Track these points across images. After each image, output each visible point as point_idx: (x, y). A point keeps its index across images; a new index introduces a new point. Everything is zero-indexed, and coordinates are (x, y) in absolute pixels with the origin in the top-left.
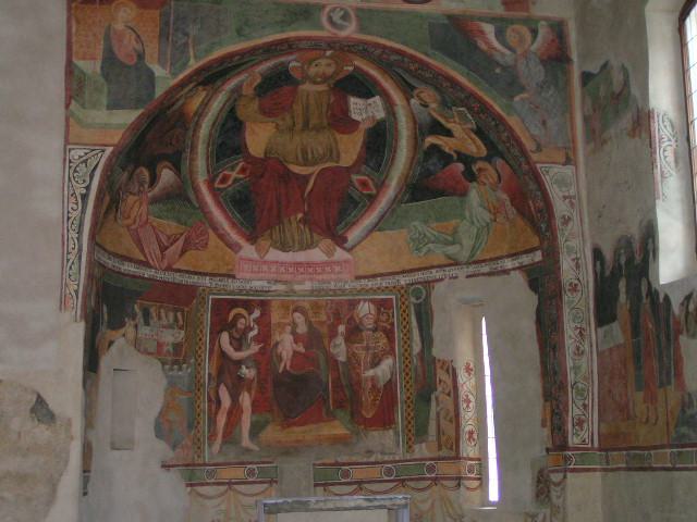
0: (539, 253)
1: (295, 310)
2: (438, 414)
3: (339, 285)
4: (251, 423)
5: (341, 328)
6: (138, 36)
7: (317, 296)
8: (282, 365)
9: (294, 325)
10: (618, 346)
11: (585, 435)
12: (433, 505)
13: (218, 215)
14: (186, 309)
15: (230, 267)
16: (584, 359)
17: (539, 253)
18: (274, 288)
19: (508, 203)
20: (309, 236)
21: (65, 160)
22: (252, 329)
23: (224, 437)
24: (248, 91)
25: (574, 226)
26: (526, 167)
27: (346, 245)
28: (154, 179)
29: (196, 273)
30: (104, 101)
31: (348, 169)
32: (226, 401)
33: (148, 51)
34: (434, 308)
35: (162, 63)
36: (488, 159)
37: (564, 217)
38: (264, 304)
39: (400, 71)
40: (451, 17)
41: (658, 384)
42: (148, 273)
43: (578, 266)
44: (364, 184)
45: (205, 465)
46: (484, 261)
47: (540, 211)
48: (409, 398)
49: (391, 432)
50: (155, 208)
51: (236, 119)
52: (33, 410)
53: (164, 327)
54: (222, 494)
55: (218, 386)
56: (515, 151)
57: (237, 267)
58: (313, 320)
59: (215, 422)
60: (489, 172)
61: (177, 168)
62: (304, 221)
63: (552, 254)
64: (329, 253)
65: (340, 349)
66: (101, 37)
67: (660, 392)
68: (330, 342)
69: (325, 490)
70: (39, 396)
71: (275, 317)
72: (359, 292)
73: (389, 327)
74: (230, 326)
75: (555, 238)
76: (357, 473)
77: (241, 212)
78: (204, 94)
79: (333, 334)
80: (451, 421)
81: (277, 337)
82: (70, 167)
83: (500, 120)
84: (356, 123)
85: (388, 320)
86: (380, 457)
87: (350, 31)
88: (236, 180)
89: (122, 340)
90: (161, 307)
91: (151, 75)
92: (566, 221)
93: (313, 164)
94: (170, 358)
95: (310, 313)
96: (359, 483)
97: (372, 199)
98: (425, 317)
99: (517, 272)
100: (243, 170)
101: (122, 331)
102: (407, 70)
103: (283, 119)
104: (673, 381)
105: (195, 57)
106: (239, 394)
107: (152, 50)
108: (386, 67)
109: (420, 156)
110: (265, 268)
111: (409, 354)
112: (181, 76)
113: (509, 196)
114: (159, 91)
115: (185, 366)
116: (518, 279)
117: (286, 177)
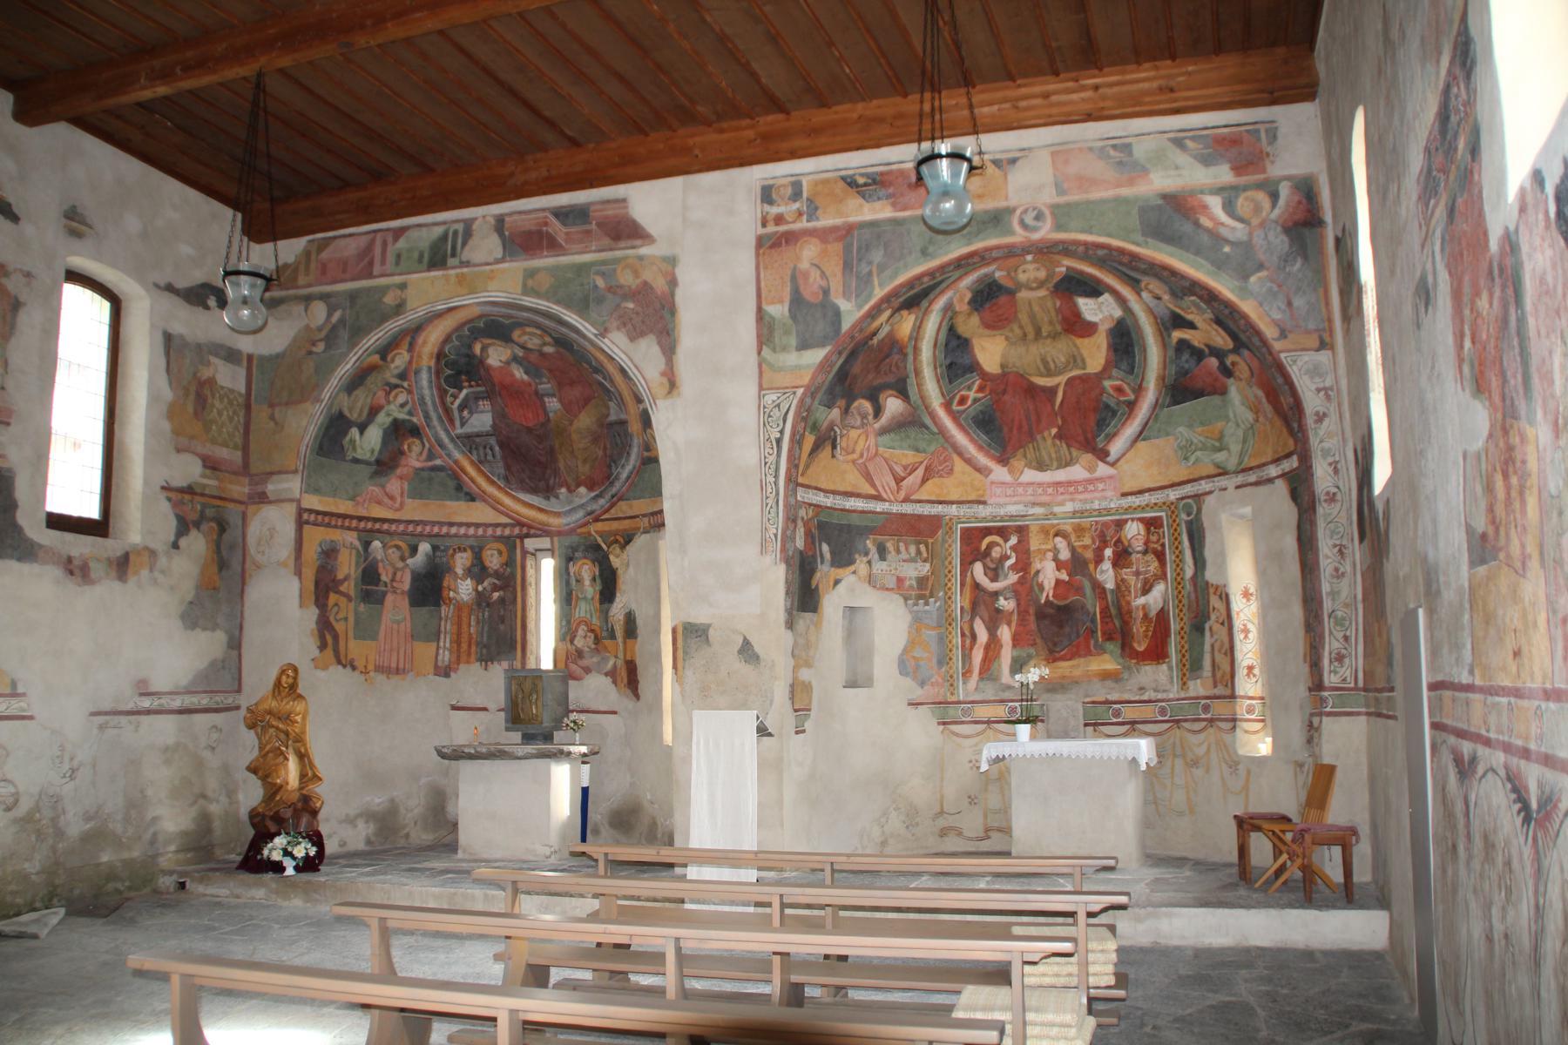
0: (1295, 458)
1: (1056, 535)
2: (1212, 646)
3: (1104, 504)
4: (1013, 658)
5: (1108, 552)
8: (1044, 595)
9: (1056, 551)
11: (1346, 672)
12: (1209, 749)
13: (960, 438)
14: (930, 541)
15: (981, 492)
16: (1345, 583)
17: (1295, 458)
19: (1264, 400)
20: (1067, 453)
22: (1008, 558)
23: (980, 674)
24: (962, 307)
27: (1109, 459)
28: (878, 411)
29: (940, 502)
30: (793, 341)
32: (983, 636)
33: (832, 289)
34: (1205, 525)
36: (1236, 350)
37: (1317, 414)
38: (1022, 531)
39: (1115, 265)
40: (1165, 197)
42: (879, 507)
43: (1336, 471)
44: (1119, 390)
45: (959, 702)
46: (1251, 469)
48: (1182, 629)
49: (1164, 667)
50: (886, 438)
51: (959, 337)
52: (740, 652)
53: (904, 561)
54: (978, 734)
55: (972, 621)
56: (1256, 340)
57: (988, 492)
58: (1076, 544)
60: (1243, 370)
61: (903, 393)
62: (1059, 436)
64: (1091, 469)
65: (1107, 575)
66: (787, 279)
68: (1096, 568)
69: (1095, 730)
70: (745, 639)
71: (1035, 543)
72: (1127, 510)
73: (1159, 548)
76: (1129, 713)
77: (987, 433)
79: (1099, 559)
80: (1225, 654)
81: (1037, 565)
82: (764, 413)
85: (1158, 540)
87: (1045, 232)
88: (976, 400)
89: (853, 578)
90: (898, 541)
91: (837, 313)
92: (1320, 418)
93: (1059, 373)
96: (1133, 723)
97: (1132, 405)
100: (981, 389)
101: (852, 568)
102: (1121, 263)
103: (1012, 331)
106: (998, 628)
107: (836, 285)
108: (1101, 263)
109: (1171, 353)
110: (1020, 490)
112: (867, 308)
113: (1264, 392)
114: (846, 325)
115: (932, 600)
116: (1281, 487)
117: (1032, 391)
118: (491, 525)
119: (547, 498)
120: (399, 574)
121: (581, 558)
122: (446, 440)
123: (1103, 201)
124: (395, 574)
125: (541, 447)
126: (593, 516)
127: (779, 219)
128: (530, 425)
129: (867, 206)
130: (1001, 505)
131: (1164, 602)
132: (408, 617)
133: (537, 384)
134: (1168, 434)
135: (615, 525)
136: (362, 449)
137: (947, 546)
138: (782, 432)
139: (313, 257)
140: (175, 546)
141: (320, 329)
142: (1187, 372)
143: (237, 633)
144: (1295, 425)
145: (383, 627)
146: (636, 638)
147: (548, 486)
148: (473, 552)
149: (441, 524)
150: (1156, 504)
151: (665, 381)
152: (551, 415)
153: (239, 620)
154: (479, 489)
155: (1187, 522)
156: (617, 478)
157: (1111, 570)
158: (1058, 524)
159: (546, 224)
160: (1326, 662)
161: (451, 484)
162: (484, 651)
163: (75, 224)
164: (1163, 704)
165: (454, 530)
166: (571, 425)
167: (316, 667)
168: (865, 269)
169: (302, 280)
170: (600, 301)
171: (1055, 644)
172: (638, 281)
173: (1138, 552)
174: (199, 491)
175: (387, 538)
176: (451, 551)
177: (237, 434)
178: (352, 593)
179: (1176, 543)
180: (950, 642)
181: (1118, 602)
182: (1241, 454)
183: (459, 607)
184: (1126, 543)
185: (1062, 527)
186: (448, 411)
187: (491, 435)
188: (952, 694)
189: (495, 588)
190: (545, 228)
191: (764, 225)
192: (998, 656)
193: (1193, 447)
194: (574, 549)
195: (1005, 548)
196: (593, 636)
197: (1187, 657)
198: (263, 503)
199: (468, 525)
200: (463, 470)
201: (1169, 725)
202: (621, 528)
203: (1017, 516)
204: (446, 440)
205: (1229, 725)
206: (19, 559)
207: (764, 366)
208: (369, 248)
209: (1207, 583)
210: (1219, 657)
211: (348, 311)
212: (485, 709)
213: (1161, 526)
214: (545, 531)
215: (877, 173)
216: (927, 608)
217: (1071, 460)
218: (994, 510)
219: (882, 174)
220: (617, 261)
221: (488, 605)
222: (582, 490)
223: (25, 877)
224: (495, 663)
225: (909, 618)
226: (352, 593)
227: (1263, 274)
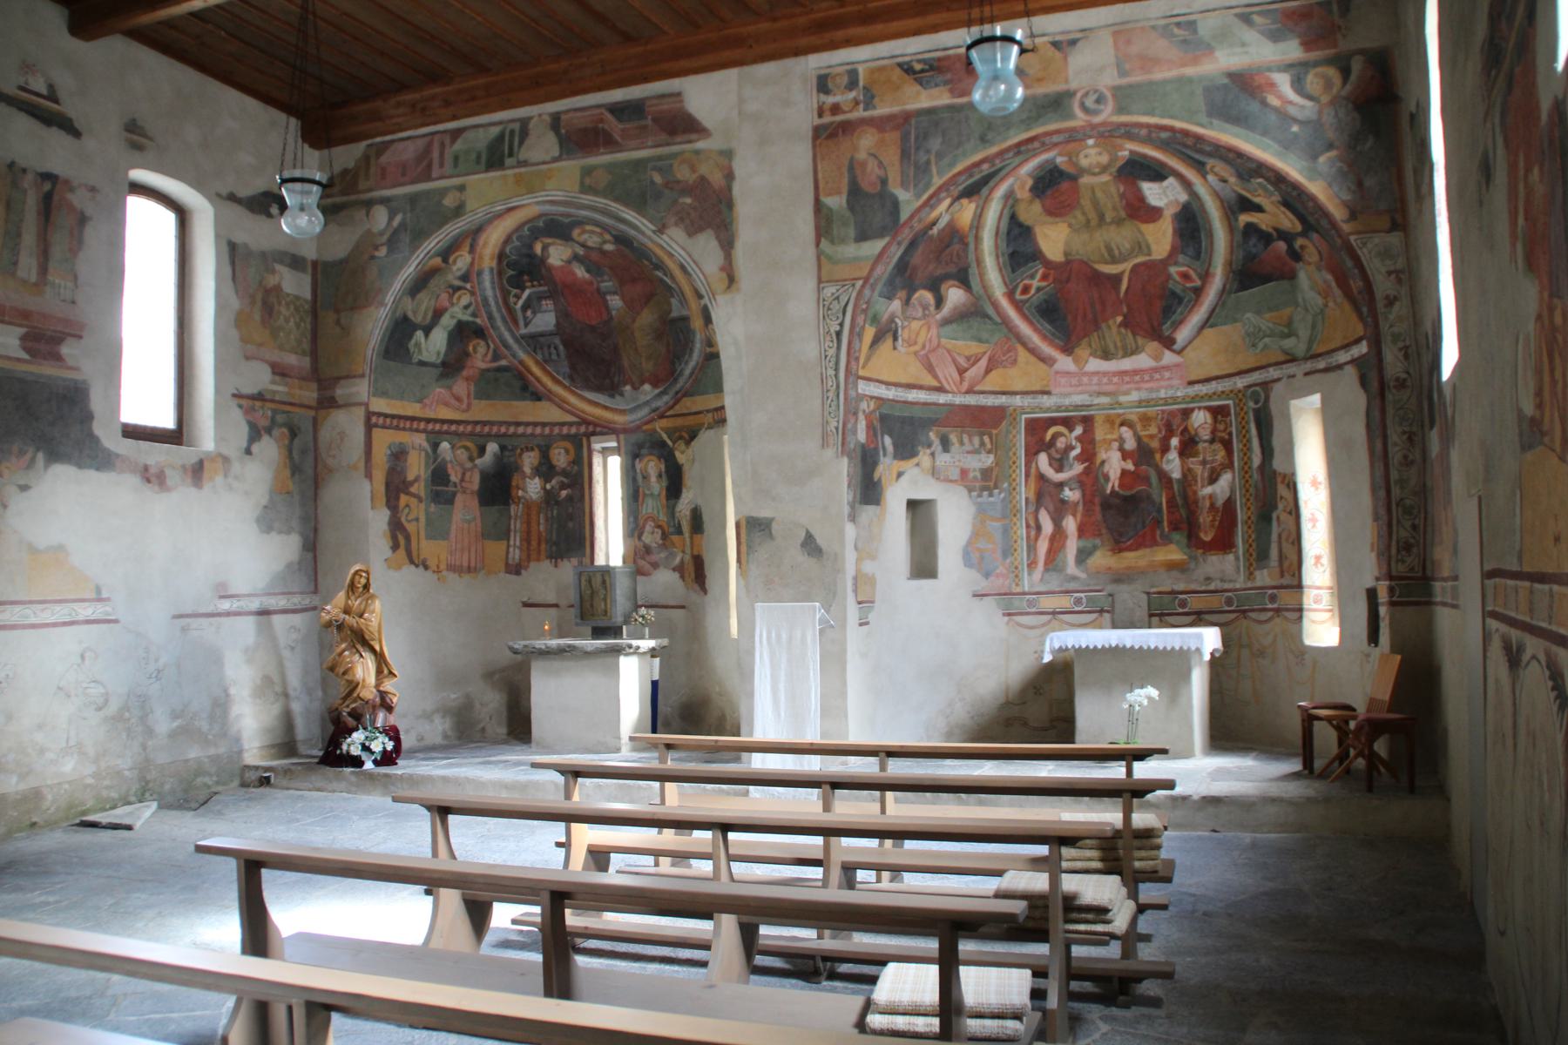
1: (1122, 424)
2: (1280, 536)
3: (1170, 393)
5: (1175, 442)
6: (881, 162)
7: (1145, 407)
8: (1110, 485)
9: (1121, 440)
13: (1024, 328)
14: (994, 432)
15: (1045, 382)
17: (1364, 343)
18: (1096, 401)
19: (1334, 284)
21: (819, 299)
22: (1073, 448)
23: (1046, 564)
24: (1023, 194)
28: (940, 302)
29: (1004, 393)
30: (852, 232)
31: (1165, 263)
35: (904, 185)
36: (1304, 234)
37: (1387, 297)
38: (1087, 421)
42: (942, 399)
44: (1185, 276)
45: (1024, 593)
48: (1249, 518)
49: (1231, 557)
50: (948, 329)
51: (1020, 225)
54: (1043, 625)
56: (1324, 222)
59: (1035, 549)
62: (1125, 324)
64: (1157, 358)
65: (1173, 464)
66: (845, 170)
68: (1162, 458)
69: (1161, 621)
70: (808, 532)
71: (1100, 433)
72: (1194, 399)
73: (1227, 437)
74: (1048, 446)
78: (973, 206)
79: (1165, 449)
80: (1293, 543)
81: (1102, 455)
82: (824, 306)
87: (1107, 114)
88: (1039, 289)
90: (962, 432)
91: (896, 205)
92: (1391, 302)
94: (977, 485)
95: (1139, 427)
97: (1198, 292)
100: (1044, 278)
101: (915, 460)
103: (1075, 217)
105: (938, 173)
107: (894, 175)
109: (1238, 237)
110: (1085, 379)
111: (1250, 468)
115: (996, 491)
116: (1351, 373)
117: (1097, 279)
119: (612, 396)
120: (468, 474)
122: (511, 341)
123: (1165, 82)
126: (657, 413)
127: (836, 109)
129: (924, 94)
130: (1068, 395)
133: (599, 282)
134: (1235, 321)
135: (679, 422)
136: (427, 350)
137: (1011, 436)
138: (841, 325)
140: (248, 452)
141: (381, 234)
143: (312, 535)
148: (540, 451)
149: (508, 424)
150: (1223, 392)
151: (724, 275)
152: (614, 313)
153: (313, 524)
155: (1254, 410)
156: (681, 374)
157: (1177, 462)
158: (1124, 414)
159: (602, 121)
162: (554, 548)
163: (135, 137)
164: (1230, 594)
165: (521, 430)
167: (389, 567)
168: (923, 157)
169: (362, 185)
170: (658, 196)
171: (1121, 535)
172: (694, 176)
173: (1205, 441)
174: (268, 397)
176: (519, 451)
177: (304, 340)
178: (422, 494)
179: (1244, 431)
180: (1015, 533)
182: (1311, 342)
183: (529, 505)
184: (1193, 432)
186: (510, 311)
188: (1017, 585)
189: (563, 486)
190: (600, 125)
192: (1063, 546)
193: (1261, 334)
197: (1254, 545)
199: (535, 424)
202: (687, 423)
203: (1082, 406)
204: (511, 341)
206: (98, 469)
207: (822, 257)
208: (427, 150)
209: (1275, 472)
213: (1229, 414)
214: (610, 429)
215: (933, 59)
216: (991, 499)
217: (1137, 348)
218: (1059, 400)
219: (939, 59)
221: (557, 503)
222: (647, 387)
223: (119, 773)
225: (973, 509)
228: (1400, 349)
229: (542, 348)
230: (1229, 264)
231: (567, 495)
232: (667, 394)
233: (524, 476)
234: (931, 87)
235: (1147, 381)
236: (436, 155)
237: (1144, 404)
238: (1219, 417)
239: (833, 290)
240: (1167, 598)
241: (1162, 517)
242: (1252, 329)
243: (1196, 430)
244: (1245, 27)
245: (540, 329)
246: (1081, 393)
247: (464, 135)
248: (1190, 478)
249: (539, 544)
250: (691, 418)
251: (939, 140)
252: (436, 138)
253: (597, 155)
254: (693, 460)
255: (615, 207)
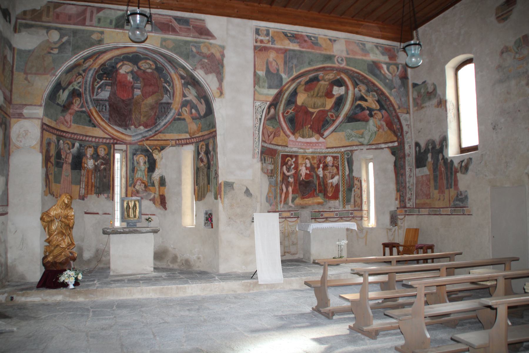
1: (306, 159)
2: (355, 195)
3: (321, 150)
5: (321, 165)
8: (302, 177)
9: (306, 164)
10: (426, 175)
11: (411, 203)
14: (274, 158)
16: (412, 178)
19: (385, 125)
22: (292, 165)
23: (284, 202)
24: (303, 83)
25: (409, 135)
26: (395, 114)
30: (266, 85)
31: (328, 111)
32: (285, 190)
33: (280, 70)
34: (354, 159)
36: (379, 110)
37: (406, 132)
38: (296, 157)
41: (445, 188)
43: (410, 148)
46: (373, 144)
47: (398, 129)
48: (344, 190)
49: (338, 201)
52: (245, 193)
53: (269, 164)
54: (283, 222)
55: (282, 184)
56: (391, 109)
58: (312, 162)
61: (275, 109)
62: (310, 128)
63: (402, 144)
64: (318, 139)
65: (320, 172)
66: (265, 63)
67: (447, 191)
69: (315, 220)
70: (247, 188)
71: (300, 161)
72: (328, 153)
73: (337, 165)
75: (403, 139)
76: (326, 215)
79: (318, 167)
80: (359, 198)
81: (300, 168)
82: (256, 108)
83: (387, 98)
84: (333, 95)
85: (337, 163)
86: (334, 210)
87: (343, 65)
88: (291, 113)
91: (281, 79)
92: (407, 133)
93: (317, 108)
96: (327, 218)
97: (334, 121)
98: (350, 163)
99: (387, 149)
100: (293, 110)
104: (453, 187)
105: (296, 71)
107: (281, 68)
109: (354, 107)
110: (297, 143)
113: (386, 123)
115: (273, 177)
118: (101, 138)
119: (126, 129)
120: (68, 155)
121: (139, 154)
122: (89, 100)
123: (359, 59)
124: (66, 155)
125: (126, 108)
126: (146, 138)
127: (262, 41)
128: (124, 99)
129: (291, 44)
131: (338, 182)
132: (70, 175)
133: (134, 83)
134: (343, 131)
135: (156, 143)
138: (261, 116)
139: (51, 9)
141: (55, 43)
142: (356, 114)
144: (399, 134)
145: (62, 178)
146: (165, 186)
147: (126, 124)
148: (94, 148)
149: (83, 135)
150: (337, 152)
151: (218, 91)
152: (135, 96)
154: (98, 122)
155: (347, 158)
156: (159, 124)
157: (322, 171)
158: (307, 155)
159: (171, 22)
160: (407, 200)
161: (88, 119)
162: (98, 190)
164: (337, 212)
165: (87, 139)
166: (143, 101)
168: (291, 65)
169: (44, 18)
170: (194, 56)
171: (304, 193)
172: (209, 52)
173: (330, 166)
175: (65, 139)
176: (86, 147)
178: (53, 162)
179: (343, 164)
181: (324, 181)
182: (369, 140)
183: (88, 171)
184: (327, 163)
185: (308, 156)
186: (93, 88)
187: (107, 101)
189: (102, 164)
190: (170, 23)
191: (256, 42)
192: (288, 196)
193: (352, 136)
194: (136, 150)
195: (292, 161)
196: (144, 185)
197: (345, 198)
198: (20, 118)
199: (93, 137)
200: (92, 113)
201: (339, 218)
202: (159, 144)
204: (89, 100)
205: (360, 218)
207: (256, 92)
208: (84, 12)
209: (354, 177)
210: (357, 199)
211: (72, 38)
212: (98, 214)
213: (338, 159)
214: (124, 142)
215: (294, 34)
217: (312, 136)
219: (296, 34)
220: (200, 43)
221: (99, 171)
222: (142, 127)
224: (102, 195)
225: (268, 183)
226: (53, 162)
227: (395, 90)
228: (409, 146)
229: (99, 106)
230: (347, 114)
231: (104, 168)
232: (151, 131)
233: (87, 158)
234: (293, 43)
235: (315, 146)
236: (88, 15)
237: (313, 153)
238: (335, 159)
239: (259, 103)
240: (317, 213)
241: (316, 188)
242: (348, 134)
243: (328, 162)
244: (376, 49)
245: (101, 98)
246: (296, 148)
247: (104, 11)
248: (325, 177)
249: (92, 187)
250: (162, 142)
251: (296, 61)
252: (89, 8)
253: (168, 34)
254: (162, 158)
255: (175, 56)
